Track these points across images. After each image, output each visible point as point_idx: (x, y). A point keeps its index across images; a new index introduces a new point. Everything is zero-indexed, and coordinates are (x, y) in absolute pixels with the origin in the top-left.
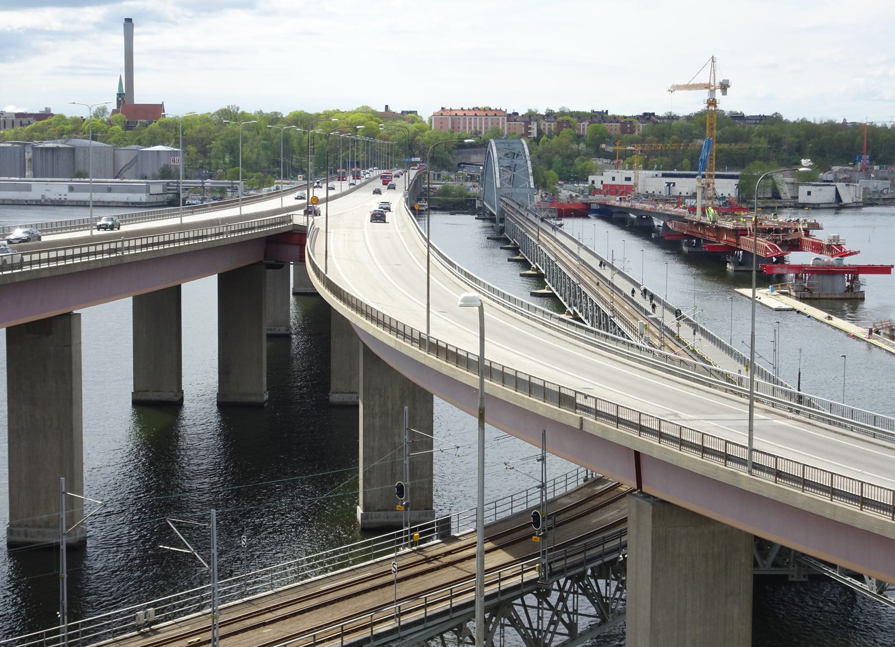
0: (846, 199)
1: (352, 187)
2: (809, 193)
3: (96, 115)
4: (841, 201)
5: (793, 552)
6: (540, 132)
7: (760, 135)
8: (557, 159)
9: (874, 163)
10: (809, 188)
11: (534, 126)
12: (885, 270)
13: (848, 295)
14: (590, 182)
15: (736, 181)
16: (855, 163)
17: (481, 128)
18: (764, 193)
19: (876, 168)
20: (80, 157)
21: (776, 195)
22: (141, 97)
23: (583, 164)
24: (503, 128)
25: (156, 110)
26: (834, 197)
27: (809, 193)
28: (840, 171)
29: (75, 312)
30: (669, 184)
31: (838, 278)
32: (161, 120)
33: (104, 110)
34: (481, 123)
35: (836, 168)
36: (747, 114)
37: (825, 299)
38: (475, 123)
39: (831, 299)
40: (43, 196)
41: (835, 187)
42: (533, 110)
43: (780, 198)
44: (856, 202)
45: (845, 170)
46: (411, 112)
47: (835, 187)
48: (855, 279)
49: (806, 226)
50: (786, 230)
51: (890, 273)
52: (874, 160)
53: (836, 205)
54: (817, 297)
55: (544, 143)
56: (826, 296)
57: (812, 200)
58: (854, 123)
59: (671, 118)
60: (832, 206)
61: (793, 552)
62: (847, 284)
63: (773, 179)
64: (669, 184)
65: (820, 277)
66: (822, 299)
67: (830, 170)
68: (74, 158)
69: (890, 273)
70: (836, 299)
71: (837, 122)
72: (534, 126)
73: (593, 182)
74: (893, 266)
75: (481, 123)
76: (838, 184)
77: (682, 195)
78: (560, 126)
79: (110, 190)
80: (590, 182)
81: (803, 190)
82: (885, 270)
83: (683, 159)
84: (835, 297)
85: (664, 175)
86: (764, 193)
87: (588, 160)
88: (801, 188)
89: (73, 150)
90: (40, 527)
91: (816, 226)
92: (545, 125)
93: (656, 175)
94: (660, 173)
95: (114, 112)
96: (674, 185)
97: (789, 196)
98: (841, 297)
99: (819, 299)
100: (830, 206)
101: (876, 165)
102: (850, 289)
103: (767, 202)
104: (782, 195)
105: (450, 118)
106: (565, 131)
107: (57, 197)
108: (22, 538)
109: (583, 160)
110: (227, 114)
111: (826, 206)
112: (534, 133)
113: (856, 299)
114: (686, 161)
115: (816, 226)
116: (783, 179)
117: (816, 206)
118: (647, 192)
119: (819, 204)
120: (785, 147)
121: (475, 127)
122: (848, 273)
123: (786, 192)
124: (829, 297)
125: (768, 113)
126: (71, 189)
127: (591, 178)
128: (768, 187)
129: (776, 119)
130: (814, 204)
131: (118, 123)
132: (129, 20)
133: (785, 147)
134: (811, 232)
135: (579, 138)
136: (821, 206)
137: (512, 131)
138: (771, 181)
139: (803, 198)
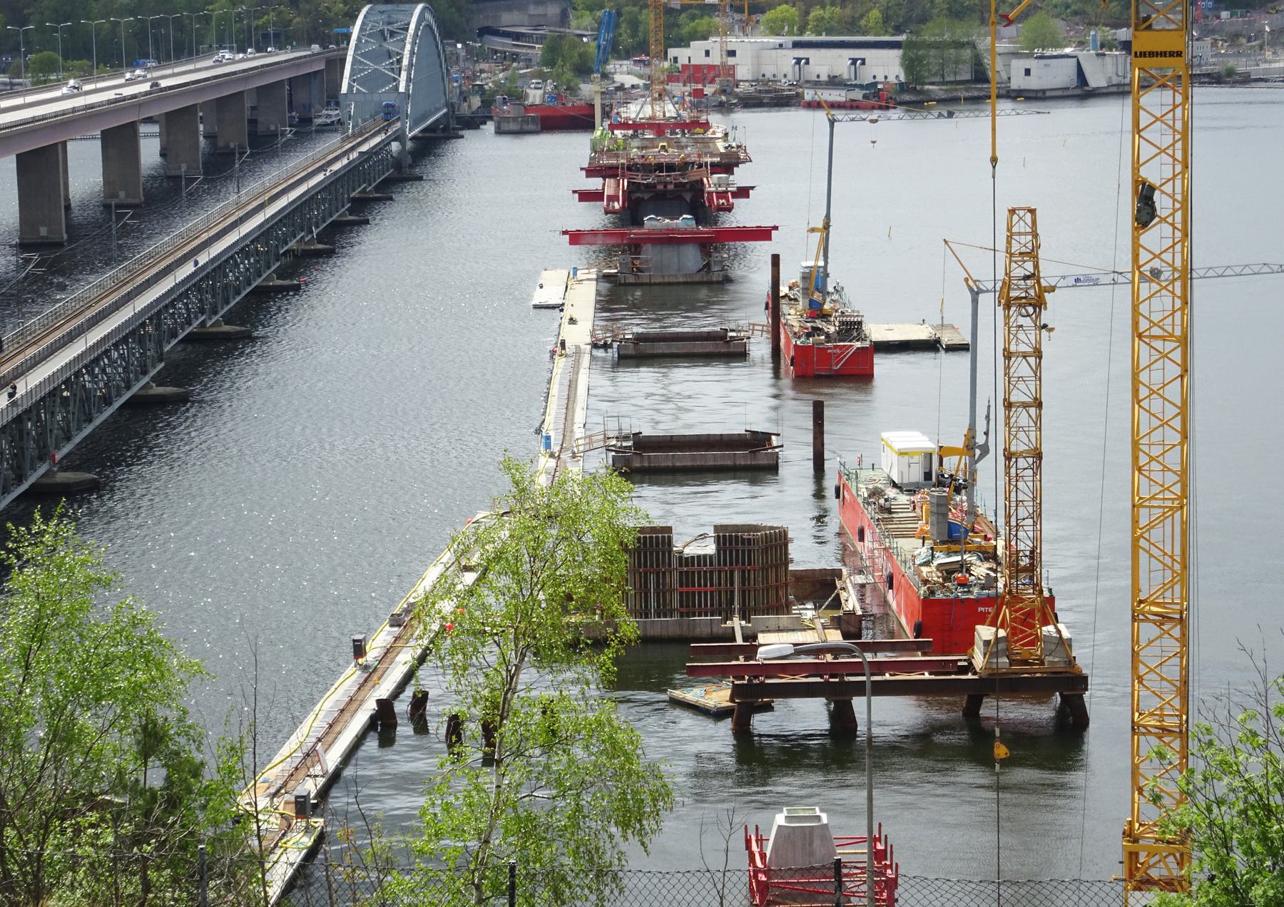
0: (1096, 80)
1: (75, 91)
2: (1028, 72)
4: (1087, 84)
5: (345, 30)
9: (1222, 5)
15: (896, 54)
18: (955, 73)
19: (1225, 14)
21: (980, 76)
23: (692, 24)
26: (1075, 77)
27: (1028, 72)
30: (854, 61)
37: (659, 284)
39: (670, 284)
41: (1075, 60)
43: (987, 81)
44: (1118, 85)
47: (1075, 60)
51: (748, 196)
53: (1078, 92)
54: (647, 281)
56: (659, 280)
57: (1033, 83)
60: (1070, 93)
61: (345, 30)
64: (854, 61)
65: (658, 248)
66: (655, 284)
70: (679, 284)
73: (676, 59)
77: (822, 79)
81: (1018, 66)
84: (675, 280)
85: (797, 45)
86: (955, 73)
87: (702, 17)
93: (781, 45)
94: (788, 40)
96: (807, 62)
98: (684, 280)
99: (650, 284)
100: (1066, 93)
101: (1227, 10)
103: (956, 90)
109: (693, 18)
111: (1059, 93)
117: (1040, 95)
118: (764, 75)
119: (1044, 91)
124: (666, 280)
128: (964, 62)
130: (1036, 91)
136: (1048, 94)
138: (969, 51)
139: (1018, 82)
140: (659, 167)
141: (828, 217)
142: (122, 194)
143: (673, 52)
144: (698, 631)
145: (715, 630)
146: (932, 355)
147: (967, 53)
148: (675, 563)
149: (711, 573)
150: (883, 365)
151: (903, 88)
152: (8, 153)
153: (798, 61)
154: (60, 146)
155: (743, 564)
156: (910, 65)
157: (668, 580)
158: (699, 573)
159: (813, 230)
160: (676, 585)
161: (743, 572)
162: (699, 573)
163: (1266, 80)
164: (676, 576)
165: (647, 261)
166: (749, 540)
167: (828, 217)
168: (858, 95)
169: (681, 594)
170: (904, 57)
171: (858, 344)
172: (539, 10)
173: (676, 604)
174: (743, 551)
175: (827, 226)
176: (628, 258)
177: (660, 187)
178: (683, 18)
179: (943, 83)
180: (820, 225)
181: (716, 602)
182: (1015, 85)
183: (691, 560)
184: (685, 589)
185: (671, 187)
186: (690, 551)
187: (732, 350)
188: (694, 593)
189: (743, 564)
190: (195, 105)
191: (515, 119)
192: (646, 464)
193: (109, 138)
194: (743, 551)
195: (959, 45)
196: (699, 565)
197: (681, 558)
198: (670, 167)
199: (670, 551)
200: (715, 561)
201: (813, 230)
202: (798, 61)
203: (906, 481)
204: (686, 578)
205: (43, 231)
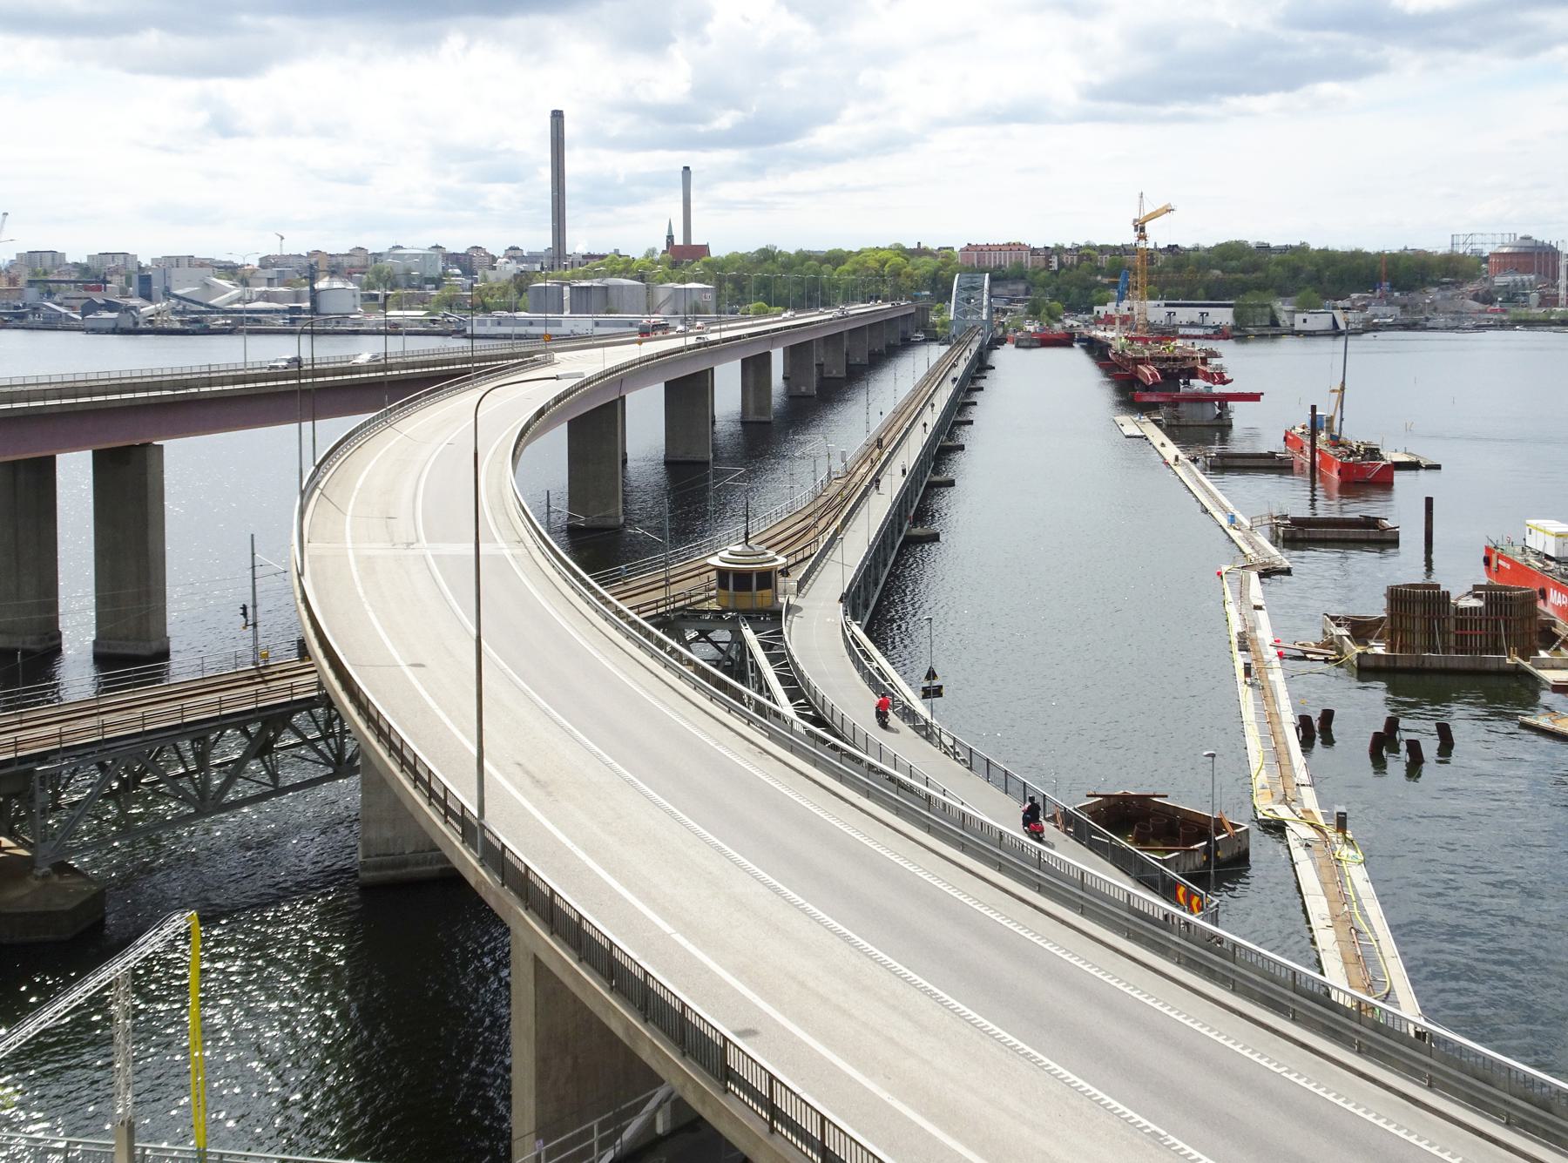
2: (1305, 321)
3: (647, 256)
6: (1061, 265)
7: (1278, 264)
8: (1074, 291)
10: (1305, 316)
11: (1055, 259)
12: (1255, 397)
13: (1216, 423)
14: (1095, 313)
15: (1231, 310)
16: (1375, 291)
17: (1005, 262)
19: (1397, 294)
20: (613, 294)
21: (1274, 322)
22: (696, 240)
24: (1027, 262)
25: (704, 249)
27: (1305, 321)
28: (1358, 298)
29: (155, 443)
30: (1202, 314)
31: (1208, 406)
32: (705, 259)
33: (653, 251)
34: (1005, 258)
35: (1354, 296)
36: (1273, 244)
38: (1000, 258)
40: (572, 331)
42: (1060, 244)
43: (1279, 326)
45: (1365, 297)
46: (947, 248)
48: (1223, 406)
49: (1203, 355)
50: (1184, 359)
51: (1259, 400)
52: (1395, 286)
55: (1063, 275)
57: (1307, 327)
58: (1326, 250)
59: (1264, 248)
62: (1218, 411)
63: (1271, 307)
64: (1202, 314)
65: (1190, 404)
67: (1349, 297)
68: (607, 296)
69: (1259, 400)
71: (1440, 251)
72: (1055, 259)
74: (1262, 394)
75: (1005, 258)
76: (1334, 311)
78: (1080, 259)
79: (531, 324)
80: (1095, 313)
81: (1299, 317)
82: (1255, 397)
83: (1197, 289)
85: (1167, 305)
88: (1297, 316)
89: (606, 288)
90: (121, 640)
91: (1215, 355)
92: (1067, 259)
94: (1162, 303)
95: (664, 252)
97: (1288, 323)
99: (1187, 426)
102: (1220, 416)
104: (1281, 322)
105: (975, 254)
106: (1085, 263)
107: (585, 332)
108: (105, 650)
109: (1100, 291)
110: (767, 255)
112: (1055, 266)
113: (1224, 426)
114: (1201, 291)
115: (1215, 355)
116: (1282, 307)
119: (1314, 331)
120: (1303, 276)
121: (995, 262)
122: (1216, 400)
123: (1284, 318)
125: (1295, 243)
126: (597, 324)
127: (1096, 308)
129: (1302, 249)
131: (816, 260)
132: (686, 168)
133: (1303, 276)
134: (1209, 360)
135: (1099, 270)
137: (1035, 264)
140: (1168, 359)
141: (1343, 383)
142: (834, 372)
143: (1096, 308)
144: (1487, 666)
145: (1501, 666)
146: (1413, 472)
147: (1268, 309)
148: (1452, 613)
149: (1481, 620)
150: (1399, 478)
151: (1234, 328)
152: (735, 359)
153: (1169, 313)
154: (619, 402)
155: (1506, 615)
156: (1236, 316)
157: (1446, 625)
158: (1471, 620)
159: (1334, 391)
160: (1452, 629)
161: (1506, 621)
162: (1471, 620)
163: (1437, 329)
164: (1453, 622)
165: (1183, 412)
166: (1511, 597)
167: (1343, 383)
168: (1210, 332)
169: (1457, 635)
170: (1234, 312)
171: (1384, 463)
172: (1014, 287)
173: (1452, 643)
174: (1506, 606)
175: (1343, 389)
176: (1171, 410)
177: (1170, 371)
178: (1094, 292)
179: (1255, 326)
180: (1338, 388)
181: (1484, 643)
182: (1297, 328)
183: (1464, 611)
184: (1459, 632)
185: (1176, 371)
186: (1463, 604)
187: (1284, 465)
188: (1466, 635)
189: (1506, 615)
190: (841, 333)
191: (1026, 340)
192: (1306, 536)
193: (674, 391)
194: (1506, 606)
195: (1264, 306)
196: (1471, 614)
197: (1457, 608)
198: (1175, 359)
199: (1449, 602)
200: (1484, 612)
201: (1334, 391)
202: (1169, 313)
203: (1561, 555)
204: (1461, 624)
205: (803, 389)
